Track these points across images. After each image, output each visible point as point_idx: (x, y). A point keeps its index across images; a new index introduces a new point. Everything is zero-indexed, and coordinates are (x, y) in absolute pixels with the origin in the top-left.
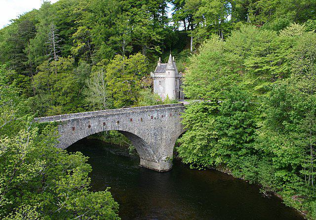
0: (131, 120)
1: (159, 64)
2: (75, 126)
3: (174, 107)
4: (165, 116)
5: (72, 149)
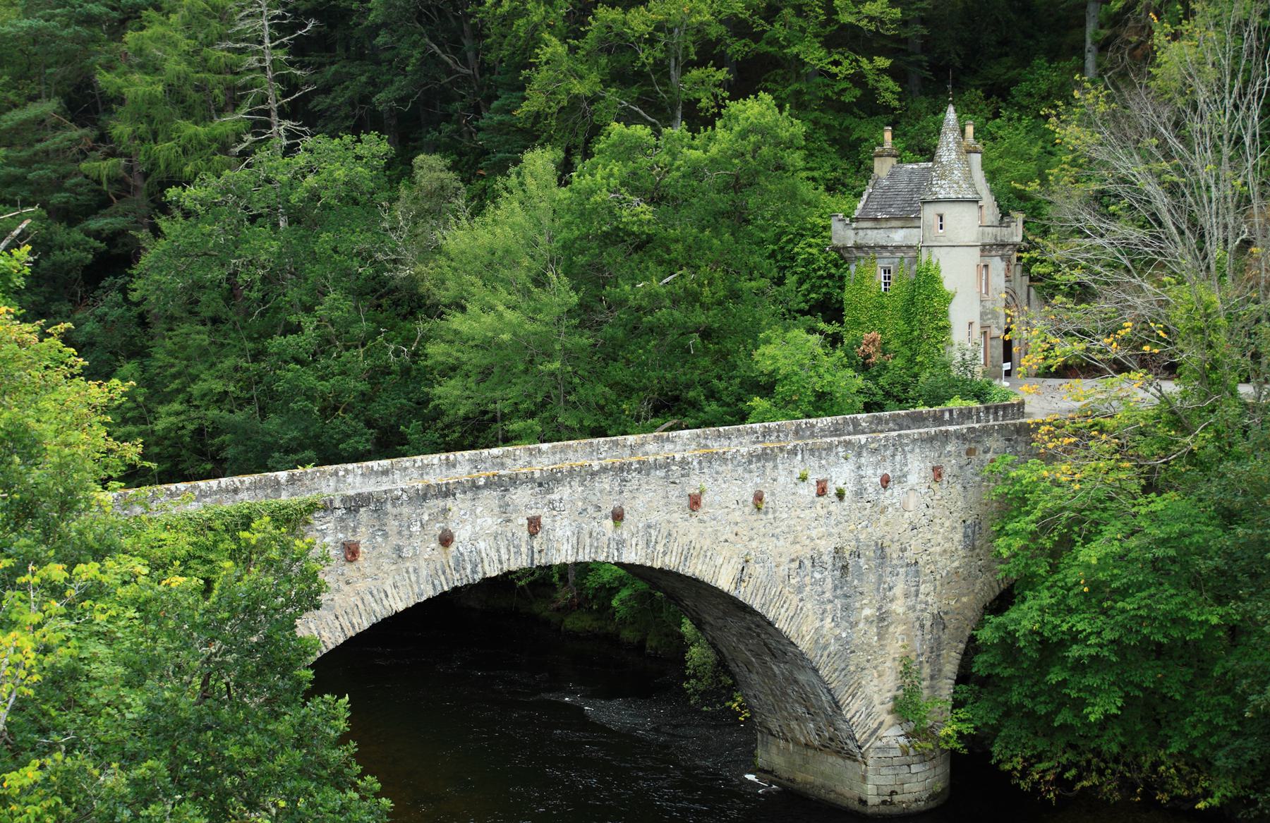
0: (695, 502)
1: (883, 168)
2: (363, 538)
3: (964, 428)
4: (902, 478)
5: (563, 182)
